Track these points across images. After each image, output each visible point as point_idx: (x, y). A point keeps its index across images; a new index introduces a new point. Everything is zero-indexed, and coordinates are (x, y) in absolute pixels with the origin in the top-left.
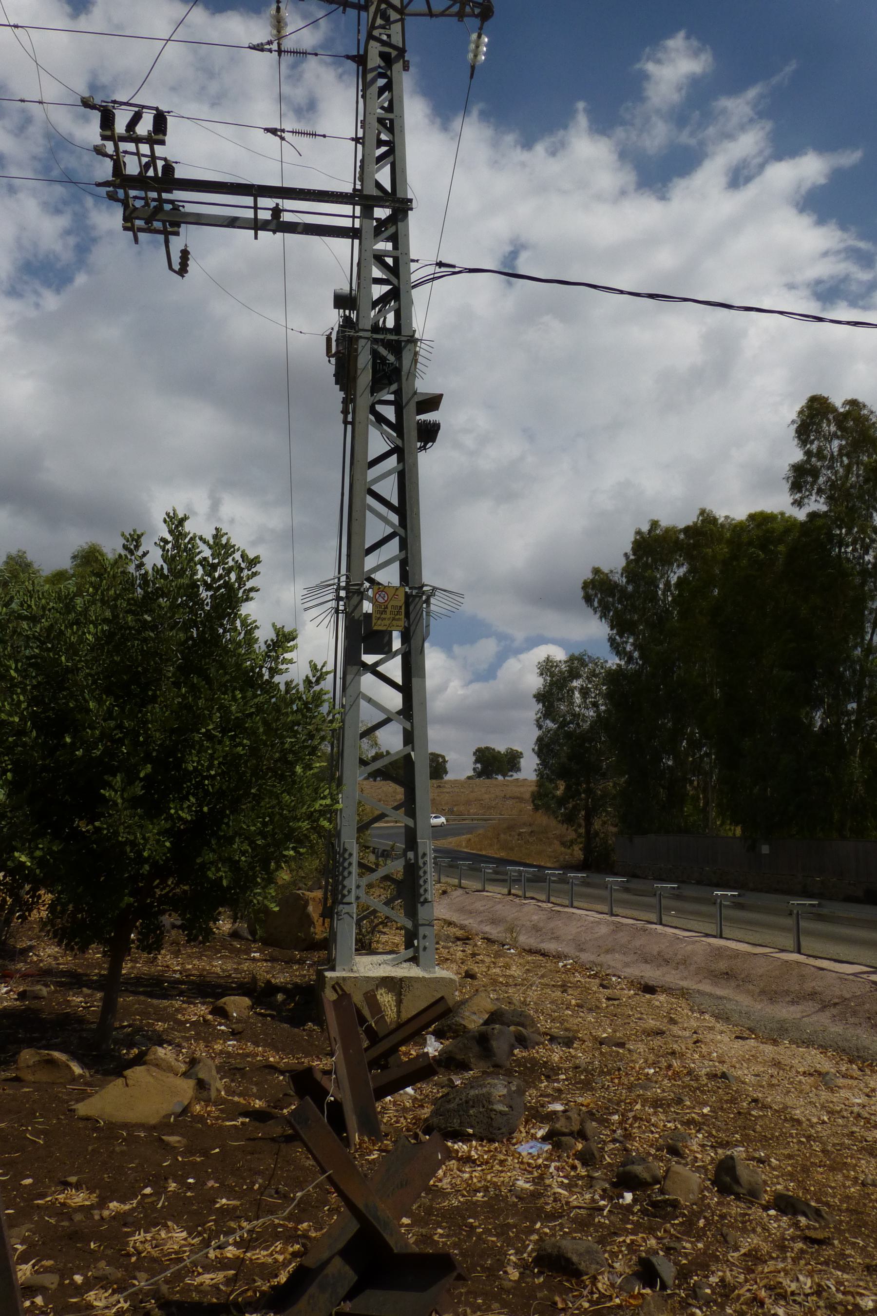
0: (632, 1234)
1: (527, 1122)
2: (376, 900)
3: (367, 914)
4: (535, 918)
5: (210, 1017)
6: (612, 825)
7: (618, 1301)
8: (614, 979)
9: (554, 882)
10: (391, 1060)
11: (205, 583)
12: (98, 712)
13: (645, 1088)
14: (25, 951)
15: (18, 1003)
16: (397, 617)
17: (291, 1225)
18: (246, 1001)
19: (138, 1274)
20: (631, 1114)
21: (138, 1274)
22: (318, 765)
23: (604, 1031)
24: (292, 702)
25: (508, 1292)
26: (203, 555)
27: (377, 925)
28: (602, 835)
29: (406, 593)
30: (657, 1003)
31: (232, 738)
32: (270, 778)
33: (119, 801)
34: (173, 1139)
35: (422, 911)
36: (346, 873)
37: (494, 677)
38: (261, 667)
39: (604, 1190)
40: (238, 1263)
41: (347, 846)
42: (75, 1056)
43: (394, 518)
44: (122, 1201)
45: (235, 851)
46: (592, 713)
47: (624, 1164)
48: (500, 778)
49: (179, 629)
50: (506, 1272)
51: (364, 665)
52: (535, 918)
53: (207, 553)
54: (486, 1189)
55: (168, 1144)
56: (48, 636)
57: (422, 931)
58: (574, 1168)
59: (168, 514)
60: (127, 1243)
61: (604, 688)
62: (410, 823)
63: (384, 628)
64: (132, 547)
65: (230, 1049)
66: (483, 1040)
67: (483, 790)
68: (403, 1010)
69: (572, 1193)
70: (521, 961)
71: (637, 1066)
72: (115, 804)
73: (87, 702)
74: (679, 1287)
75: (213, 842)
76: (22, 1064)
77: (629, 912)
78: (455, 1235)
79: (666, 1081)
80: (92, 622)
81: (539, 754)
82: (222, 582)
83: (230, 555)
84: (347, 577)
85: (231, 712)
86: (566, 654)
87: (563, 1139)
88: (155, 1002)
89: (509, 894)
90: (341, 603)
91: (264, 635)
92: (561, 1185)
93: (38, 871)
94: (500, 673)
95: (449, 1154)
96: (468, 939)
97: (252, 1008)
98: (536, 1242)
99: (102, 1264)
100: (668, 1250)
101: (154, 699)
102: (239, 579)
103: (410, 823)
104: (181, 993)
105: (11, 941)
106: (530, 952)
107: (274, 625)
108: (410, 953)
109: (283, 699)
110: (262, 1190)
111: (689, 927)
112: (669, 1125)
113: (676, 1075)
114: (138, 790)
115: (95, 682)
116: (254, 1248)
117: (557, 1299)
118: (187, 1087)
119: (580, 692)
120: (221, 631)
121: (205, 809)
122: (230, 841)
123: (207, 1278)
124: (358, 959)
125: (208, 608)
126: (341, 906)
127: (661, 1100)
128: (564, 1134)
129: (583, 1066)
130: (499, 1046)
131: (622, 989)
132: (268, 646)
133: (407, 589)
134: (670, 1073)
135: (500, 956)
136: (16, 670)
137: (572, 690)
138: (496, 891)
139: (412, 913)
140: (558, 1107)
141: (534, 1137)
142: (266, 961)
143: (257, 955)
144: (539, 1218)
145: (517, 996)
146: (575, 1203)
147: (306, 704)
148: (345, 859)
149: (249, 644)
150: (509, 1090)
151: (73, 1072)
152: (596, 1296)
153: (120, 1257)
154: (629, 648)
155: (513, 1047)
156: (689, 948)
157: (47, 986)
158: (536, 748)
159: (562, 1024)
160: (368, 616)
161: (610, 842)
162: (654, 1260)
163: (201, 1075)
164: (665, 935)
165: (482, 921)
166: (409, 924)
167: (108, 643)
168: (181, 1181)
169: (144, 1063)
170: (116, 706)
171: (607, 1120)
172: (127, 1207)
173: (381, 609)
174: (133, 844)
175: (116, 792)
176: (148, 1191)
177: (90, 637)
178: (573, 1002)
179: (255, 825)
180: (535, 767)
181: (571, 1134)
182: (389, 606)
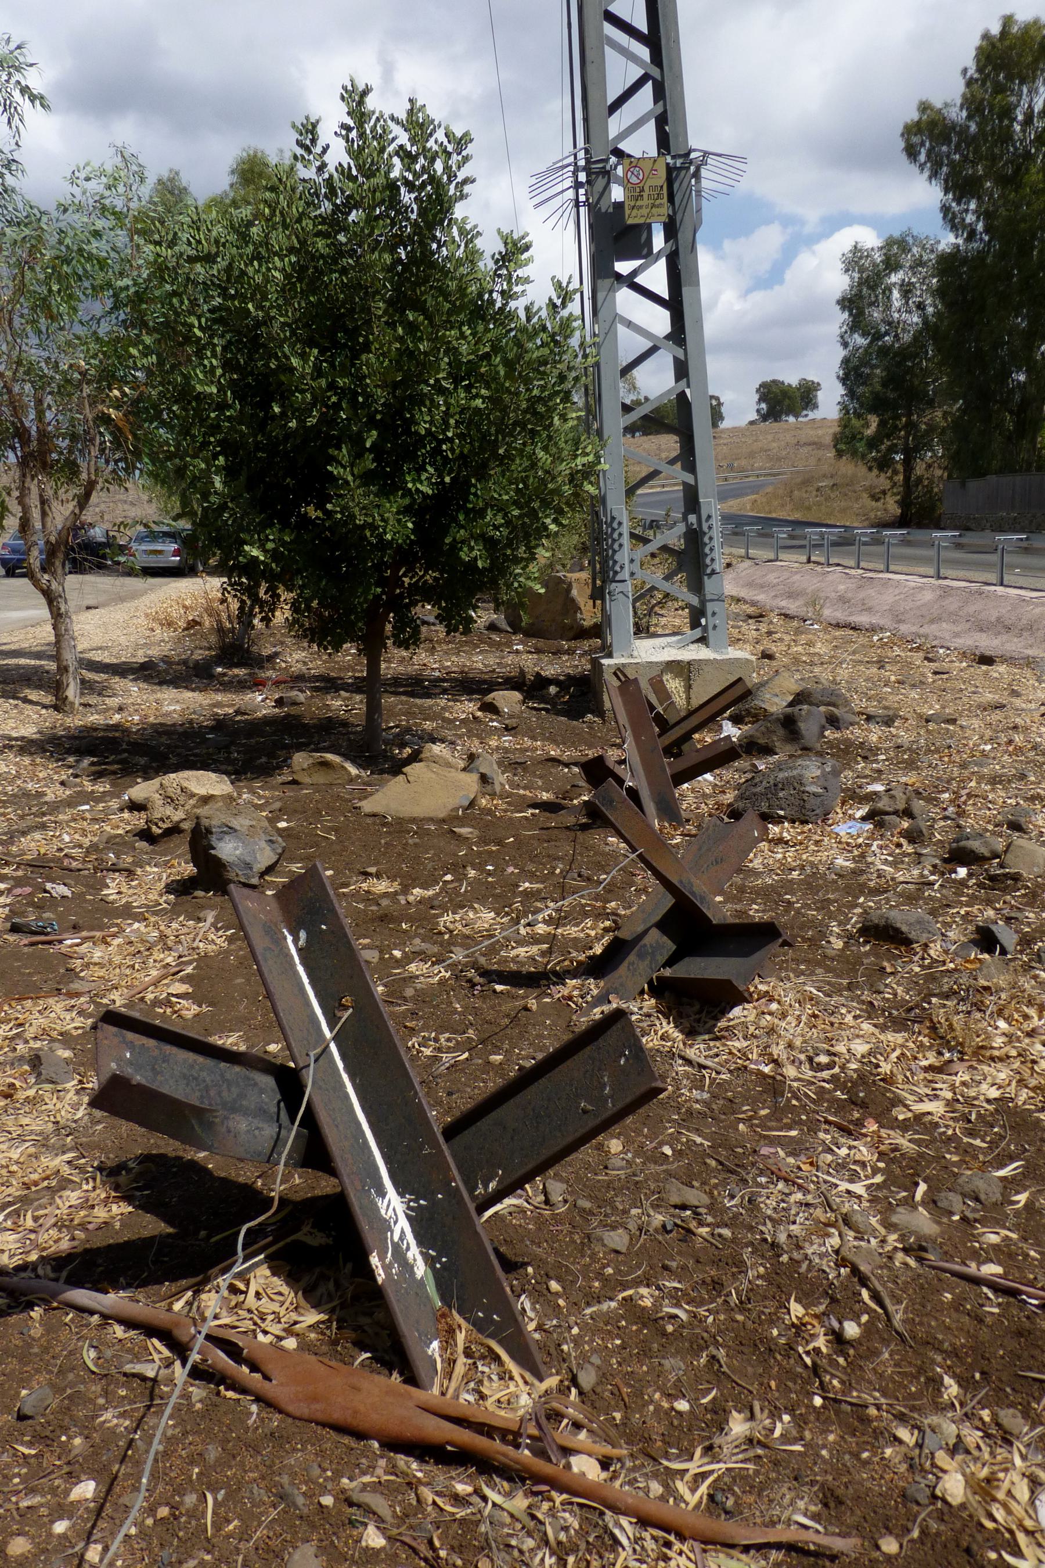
0: (967, 906)
1: (843, 803)
2: (655, 576)
3: (644, 594)
4: (842, 587)
5: (479, 714)
6: (940, 467)
7: (952, 965)
8: (941, 651)
9: (865, 544)
10: (685, 747)
11: (407, 183)
12: (304, 368)
13: (980, 765)
14: (271, 658)
15: (277, 710)
16: (658, 202)
17: (598, 904)
18: (517, 696)
19: (453, 949)
20: (964, 792)
21: (453, 949)
22: (574, 415)
23: (931, 707)
24: (536, 333)
25: (833, 959)
26: (398, 142)
27: (653, 606)
28: (926, 483)
29: (668, 164)
30: (996, 675)
31: (468, 388)
32: (519, 433)
33: (350, 478)
34: (464, 831)
35: (709, 584)
36: (616, 546)
37: (781, 281)
38: (491, 292)
39: (935, 866)
40: (551, 938)
41: (614, 514)
42: (346, 756)
43: (643, 52)
44: (425, 887)
45: (488, 525)
46: (915, 319)
47: (957, 840)
48: (791, 419)
49: (383, 250)
50: (829, 942)
51: (618, 277)
52: (842, 587)
53: (403, 138)
54: (802, 868)
55: (460, 836)
56: (228, 280)
57: (710, 607)
58: (899, 845)
59: (345, 88)
60: (438, 923)
61: (935, 280)
62: (690, 479)
63: (641, 221)
64: (308, 142)
65: (507, 744)
66: (789, 723)
67: (770, 437)
68: (692, 696)
69: (898, 870)
70: (828, 637)
71: (971, 743)
72: (347, 482)
73: (288, 358)
74: (1021, 952)
75: (461, 517)
76: (296, 768)
77: (961, 574)
78: (772, 910)
79: (1006, 757)
80: (276, 254)
81: (844, 380)
82: (426, 176)
83: (431, 135)
84: (587, 151)
85: (460, 354)
86: (879, 237)
87: (886, 817)
88: (418, 701)
89: (809, 561)
90: (582, 191)
91: (489, 246)
92: (886, 862)
93: (274, 565)
94: (788, 275)
95: (764, 836)
96: (762, 616)
97: (524, 702)
98: (860, 915)
99: (417, 941)
100: (1008, 920)
101: (366, 347)
102: (447, 168)
103: (690, 479)
104: (445, 691)
105: (255, 649)
106: (838, 626)
107: (499, 231)
108: (698, 633)
109: (523, 330)
110: (564, 875)
111: (1039, 586)
112: (1009, 801)
113: (1019, 750)
114: (369, 463)
115: (293, 333)
116: (564, 925)
117: (885, 964)
118: (471, 781)
119: (900, 290)
120: (434, 246)
121: (447, 479)
122: (481, 513)
123: (522, 951)
124: (638, 643)
125: (414, 216)
126: (614, 585)
127: (1001, 776)
128: (887, 813)
129: (906, 745)
130: (808, 728)
131: (952, 661)
132: (497, 262)
133: (669, 159)
134: (1011, 749)
135: (802, 633)
136: (200, 327)
137: (889, 289)
138: (792, 560)
139: (697, 586)
140: (879, 787)
141: (851, 817)
142: (530, 652)
143: (520, 647)
144: (862, 893)
145: (824, 675)
146: (902, 879)
147: (553, 336)
148: (614, 530)
149: (472, 261)
150: (824, 770)
151: (349, 773)
152: (927, 962)
153: (434, 934)
154: (970, 218)
155: (823, 728)
156: (1038, 610)
157: (302, 691)
158: (841, 373)
159: (879, 702)
160: (619, 206)
161: (936, 490)
162: (994, 928)
163: (482, 770)
164: (1006, 597)
165: (776, 596)
166: (695, 601)
167: (300, 280)
168: (480, 868)
169: (421, 761)
170: (325, 361)
171: (936, 799)
172: (431, 893)
173: (636, 193)
174: (373, 527)
175: (344, 467)
176: (448, 877)
177: (277, 274)
178: (893, 678)
179: (507, 493)
180: (839, 399)
181: (896, 813)
182: (646, 188)
